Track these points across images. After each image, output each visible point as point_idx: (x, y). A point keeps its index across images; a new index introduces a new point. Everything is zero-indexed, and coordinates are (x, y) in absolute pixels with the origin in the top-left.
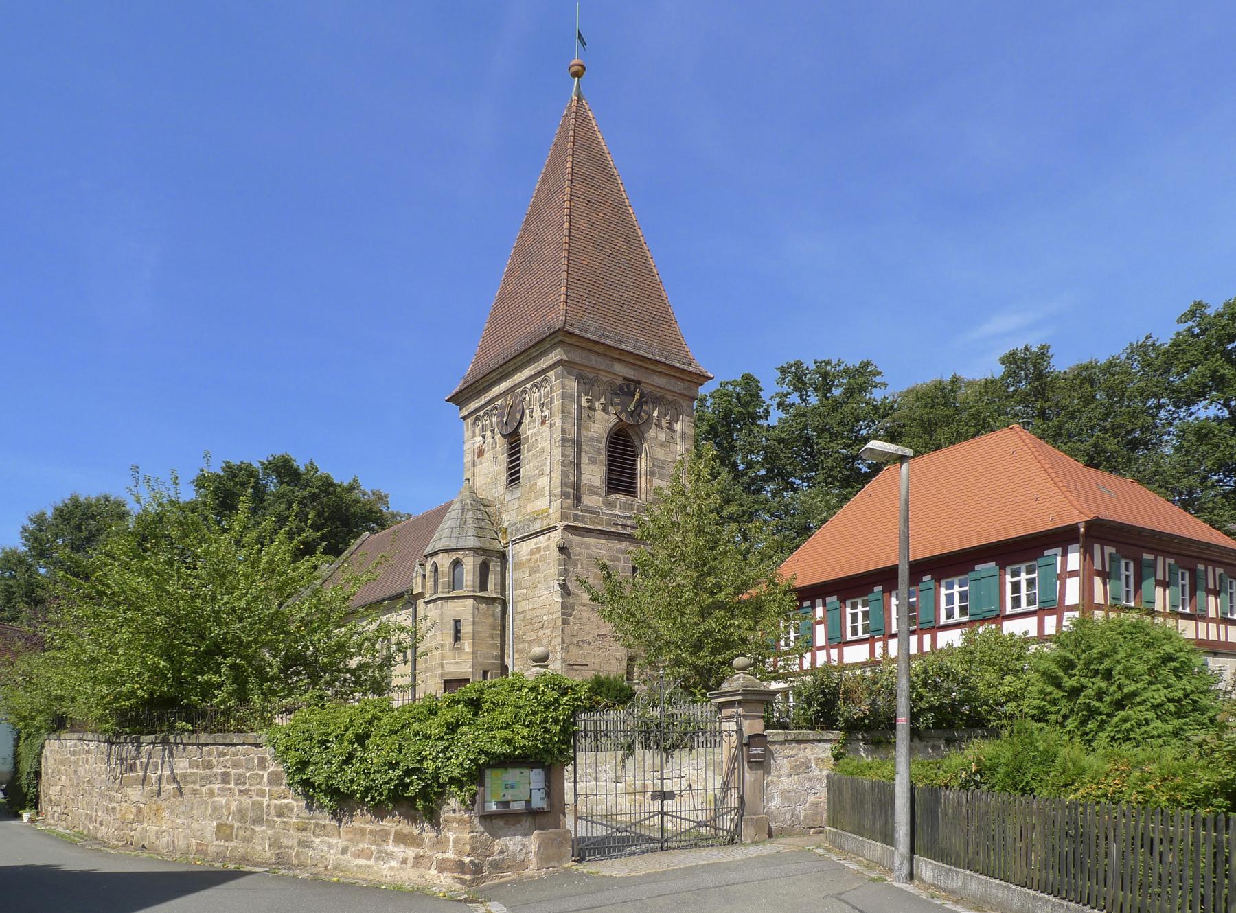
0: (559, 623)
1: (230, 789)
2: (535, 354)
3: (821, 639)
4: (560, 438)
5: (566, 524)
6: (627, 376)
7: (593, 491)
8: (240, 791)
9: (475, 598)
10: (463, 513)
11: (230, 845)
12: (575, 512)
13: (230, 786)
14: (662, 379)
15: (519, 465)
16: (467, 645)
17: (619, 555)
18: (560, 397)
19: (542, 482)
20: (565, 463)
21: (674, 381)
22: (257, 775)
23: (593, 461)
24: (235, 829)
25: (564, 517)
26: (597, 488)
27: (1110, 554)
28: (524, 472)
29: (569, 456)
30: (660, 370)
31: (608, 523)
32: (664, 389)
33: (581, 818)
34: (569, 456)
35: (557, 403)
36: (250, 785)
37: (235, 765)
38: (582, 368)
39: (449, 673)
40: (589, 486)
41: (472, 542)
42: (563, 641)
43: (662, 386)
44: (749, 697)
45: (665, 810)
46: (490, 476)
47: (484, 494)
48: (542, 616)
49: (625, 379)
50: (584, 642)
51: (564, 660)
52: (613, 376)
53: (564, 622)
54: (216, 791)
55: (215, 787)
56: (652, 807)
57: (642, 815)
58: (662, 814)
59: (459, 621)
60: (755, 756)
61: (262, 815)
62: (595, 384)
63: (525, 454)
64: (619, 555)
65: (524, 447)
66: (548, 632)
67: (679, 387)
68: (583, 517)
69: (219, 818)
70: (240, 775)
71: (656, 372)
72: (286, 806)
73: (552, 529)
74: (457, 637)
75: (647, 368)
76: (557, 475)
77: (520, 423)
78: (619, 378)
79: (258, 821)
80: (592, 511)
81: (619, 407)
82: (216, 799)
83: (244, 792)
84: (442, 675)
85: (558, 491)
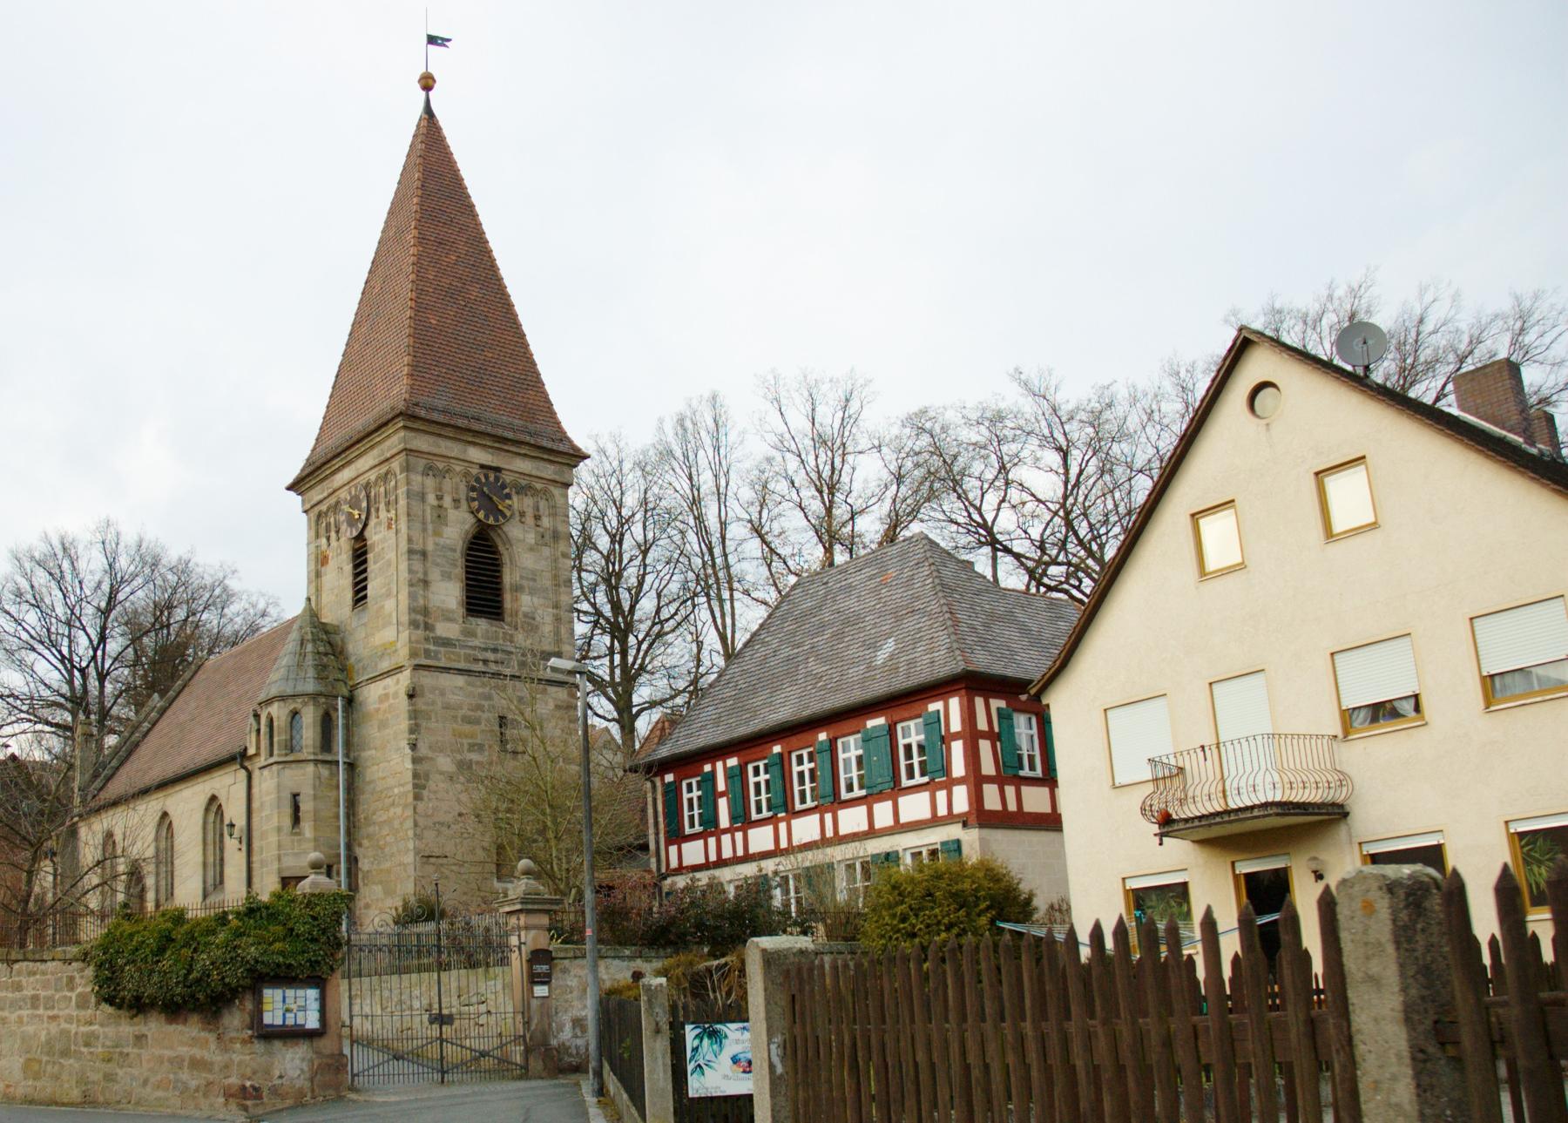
0: (411, 796)
1: (39, 1016)
2: (378, 439)
3: (724, 822)
4: (405, 549)
5: (416, 662)
6: (484, 463)
7: (447, 617)
8: (49, 1017)
9: (316, 762)
10: (302, 644)
11: (39, 1084)
12: (427, 646)
13: (38, 1012)
14: (526, 462)
15: (366, 579)
16: (307, 828)
17: (483, 702)
18: (405, 495)
19: (390, 605)
20: (414, 581)
21: (542, 464)
22: (65, 997)
23: (447, 576)
24: (43, 1065)
25: (413, 654)
26: (452, 611)
27: (999, 709)
28: (370, 591)
29: (417, 572)
30: (523, 452)
31: (467, 658)
32: (530, 476)
33: (357, 1042)
34: (417, 572)
35: (402, 502)
36: (60, 1009)
37: (45, 987)
38: (430, 457)
39: (289, 868)
40: (443, 610)
41: (310, 686)
42: (416, 825)
43: (526, 472)
44: (530, 907)
45: (444, 1036)
46: (336, 591)
47: (327, 617)
48: (391, 788)
49: (482, 466)
50: (442, 824)
51: (417, 852)
52: (466, 464)
53: (417, 797)
54: (25, 1019)
55: (25, 1013)
56: (429, 1032)
57: (420, 1041)
58: (441, 1040)
59: (298, 795)
60: (539, 975)
61: (70, 1045)
62: (447, 475)
63: (373, 567)
64: (483, 702)
65: (370, 556)
66: (399, 810)
67: (549, 471)
68: (437, 653)
69: (29, 1052)
70: (51, 998)
71: (519, 454)
72: (93, 1033)
73: (399, 669)
74: (296, 820)
75: (508, 451)
76: (404, 597)
77: (365, 525)
78: (474, 466)
79: (65, 1053)
80: (446, 642)
81: (476, 503)
82: (25, 1028)
83: (53, 1018)
84: (280, 870)
85: (405, 618)
